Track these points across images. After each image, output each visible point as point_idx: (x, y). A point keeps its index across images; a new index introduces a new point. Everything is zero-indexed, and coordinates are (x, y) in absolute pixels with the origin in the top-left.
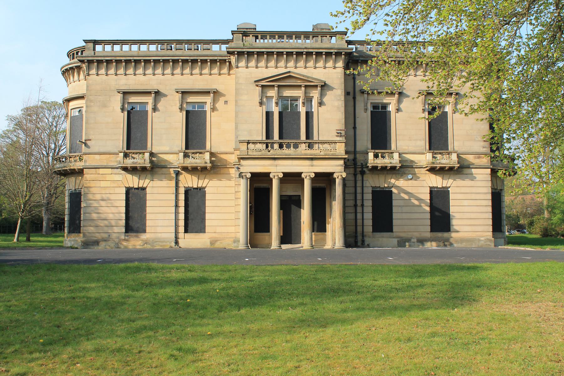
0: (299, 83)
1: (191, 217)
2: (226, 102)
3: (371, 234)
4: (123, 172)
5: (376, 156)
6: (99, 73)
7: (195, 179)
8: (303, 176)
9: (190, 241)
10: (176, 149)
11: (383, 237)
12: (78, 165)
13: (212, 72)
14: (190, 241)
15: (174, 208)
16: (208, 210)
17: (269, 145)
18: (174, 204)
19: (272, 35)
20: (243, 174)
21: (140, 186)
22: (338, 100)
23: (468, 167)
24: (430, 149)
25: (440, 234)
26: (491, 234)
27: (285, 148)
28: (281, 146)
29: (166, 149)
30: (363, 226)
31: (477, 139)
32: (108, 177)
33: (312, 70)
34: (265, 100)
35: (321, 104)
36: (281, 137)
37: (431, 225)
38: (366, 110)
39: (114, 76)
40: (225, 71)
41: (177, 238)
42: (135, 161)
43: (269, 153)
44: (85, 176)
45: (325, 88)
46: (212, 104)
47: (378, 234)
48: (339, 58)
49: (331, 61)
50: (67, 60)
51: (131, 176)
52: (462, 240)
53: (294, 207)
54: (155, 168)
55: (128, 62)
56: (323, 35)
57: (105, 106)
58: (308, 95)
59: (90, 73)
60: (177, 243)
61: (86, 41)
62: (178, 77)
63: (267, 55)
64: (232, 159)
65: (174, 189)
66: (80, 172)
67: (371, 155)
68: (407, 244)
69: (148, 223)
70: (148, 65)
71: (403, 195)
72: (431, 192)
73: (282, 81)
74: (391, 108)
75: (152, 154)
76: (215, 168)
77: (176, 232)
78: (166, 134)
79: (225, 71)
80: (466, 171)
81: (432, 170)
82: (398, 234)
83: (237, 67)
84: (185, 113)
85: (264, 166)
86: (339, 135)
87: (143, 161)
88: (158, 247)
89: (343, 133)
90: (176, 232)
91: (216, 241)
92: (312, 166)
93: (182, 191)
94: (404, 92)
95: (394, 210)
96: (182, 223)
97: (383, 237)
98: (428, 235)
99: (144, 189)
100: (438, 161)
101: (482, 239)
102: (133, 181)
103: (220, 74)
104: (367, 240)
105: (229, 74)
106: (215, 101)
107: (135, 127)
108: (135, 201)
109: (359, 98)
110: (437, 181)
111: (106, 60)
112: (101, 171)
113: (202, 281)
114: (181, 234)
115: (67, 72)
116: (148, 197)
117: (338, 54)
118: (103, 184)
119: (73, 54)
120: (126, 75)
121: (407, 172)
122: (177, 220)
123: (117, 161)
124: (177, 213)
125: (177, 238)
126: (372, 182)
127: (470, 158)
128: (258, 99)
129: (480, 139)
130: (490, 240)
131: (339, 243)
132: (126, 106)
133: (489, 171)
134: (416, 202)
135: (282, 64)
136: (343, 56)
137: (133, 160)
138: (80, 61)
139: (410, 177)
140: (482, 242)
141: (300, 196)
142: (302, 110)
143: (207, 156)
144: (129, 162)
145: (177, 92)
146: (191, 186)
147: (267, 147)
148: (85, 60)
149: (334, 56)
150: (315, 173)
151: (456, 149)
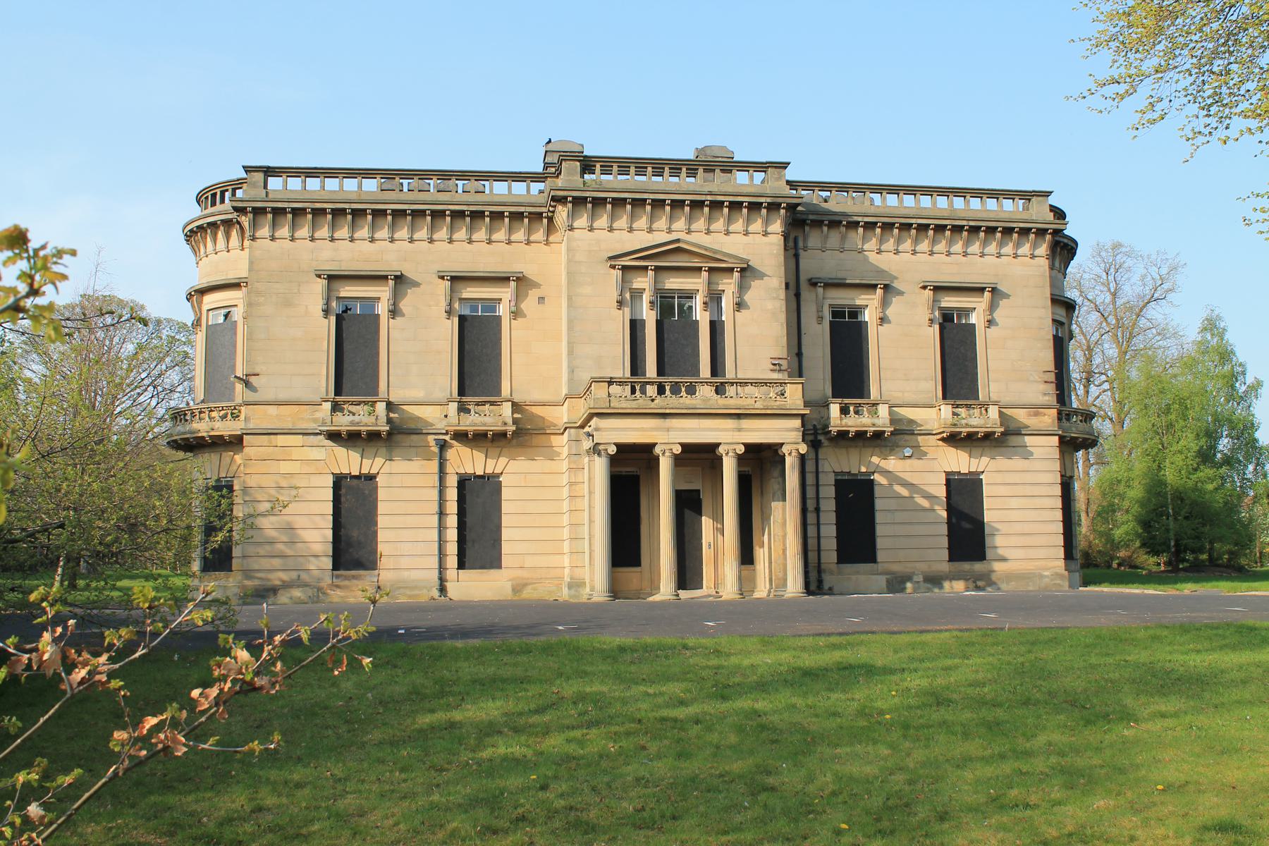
0: (696, 262)
1: (470, 536)
2: (541, 300)
3: (834, 567)
4: (329, 443)
5: (844, 411)
6: (277, 234)
7: (479, 456)
8: (657, 450)
9: (472, 587)
10: (441, 395)
11: (858, 573)
12: (226, 428)
13: (513, 238)
14: (472, 587)
15: (436, 517)
16: (505, 521)
17: (638, 388)
18: (435, 508)
19: (624, 165)
20: (601, 447)
21: (365, 471)
22: (775, 298)
23: (1018, 433)
24: (944, 398)
25: (966, 566)
26: (1061, 563)
27: (683, 393)
28: (661, 391)
29: (419, 394)
30: (819, 550)
32: (296, 453)
33: (721, 237)
35: (740, 306)
36: (661, 372)
37: (950, 548)
39: (347, 242)
40: (539, 235)
41: (442, 580)
42: (356, 418)
43: (653, 405)
44: (246, 450)
45: (748, 274)
46: (513, 303)
47: (848, 568)
48: (774, 215)
49: (760, 221)
50: (196, 211)
51: (343, 450)
52: (1010, 577)
54: (396, 435)
55: (338, 213)
56: (710, 167)
57: (288, 303)
58: (713, 287)
59: (258, 234)
60: (443, 590)
61: (248, 169)
62: (442, 246)
63: (633, 206)
64: (561, 415)
65: (437, 477)
66: (236, 442)
67: (835, 409)
68: (909, 585)
70: (439, 222)
71: (898, 488)
73: (664, 259)
74: (869, 316)
75: (390, 406)
76: (523, 435)
77: (440, 567)
78: (417, 363)
79: (539, 235)
80: (1014, 440)
81: (953, 439)
82: (886, 566)
83: (571, 229)
84: (456, 320)
85: (642, 429)
87: (372, 419)
88: (403, 600)
89: (784, 364)
90: (442, 568)
91: (525, 585)
92: (740, 430)
93: (452, 481)
94: (895, 284)
95: (879, 517)
96: (452, 548)
97: (858, 573)
98: (945, 567)
99: (371, 478)
102: (350, 461)
103: (528, 243)
104: (828, 581)
105: (547, 243)
106: (519, 297)
107: (354, 351)
108: (353, 505)
109: (806, 294)
110: (960, 461)
111: (293, 209)
112: (281, 440)
113: (849, 673)
115: (195, 234)
116: (381, 494)
117: (773, 207)
118: (285, 467)
119: (214, 195)
120: (332, 239)
121: (901, 443)
122: (442, 542)
123: (315, 420)
124: (442, 528)
125: (442, 580)
127: (1021, 415)
128: (615, 295)
130: (1061, 576)
131: (794, 585)
132: (334, 304)
133: (1055, 440)
134: (925, 503)
135: (662, 223)
136: (783, 212)
137: (351, 418)
138: (236, 209)
139: (908, 452)
141: (698, 491)
142: (702, 316)
143: (507, 409)
144: (343, 422)
145: (442, 278)
146: (346, 471)
147: (633, 391)
148: (241, 208)
149: (687, 209)
150: (745, 445)
151: (994, 397)
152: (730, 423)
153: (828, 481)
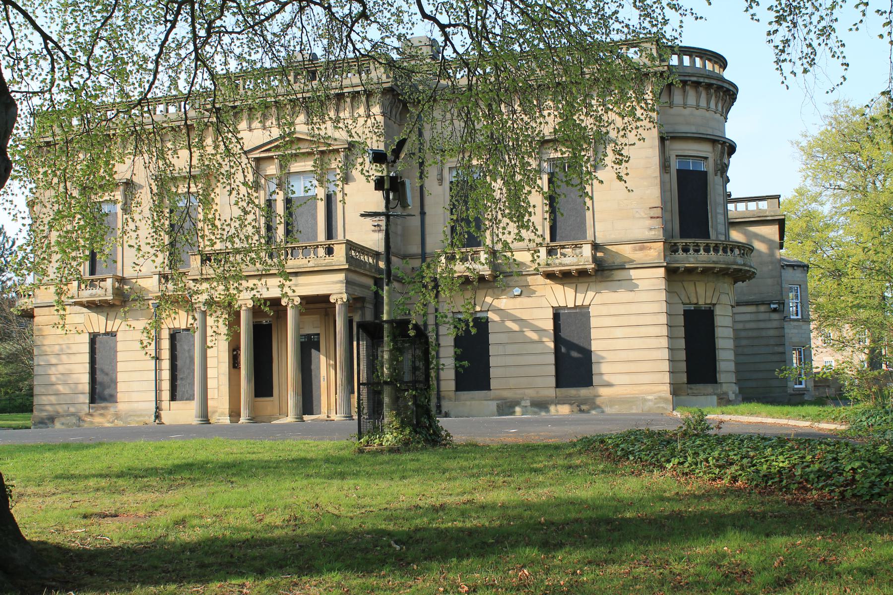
3: (452, 394)
11: (473, 399)
25: (572, 392)
31: (637, 215)
34: (263, 181)
37: (689, 372)
38: (441, 180)
41: (158, 408)
44: (36, 319)
53: (313, 351)
54: (123, 300)
60: (158, 416)
69: (120, 387)
72: (556, 317)
75: (596, 247)
86: (376, 228)
90: (158, 400)
93: (165, 334)
95: (492, 350)
96: (166, 385)
97: (473, 400)
99: (113, 334)
100: (557, 261)
101: (650, 397)
104: (446, 406)
114: (165, 404)
116: (120, 347)
125: (158, 408)
129: (643, 214)
130: (665, 400)
133: (661, 272)
139: (517, 291)
140: (650, 403)
146: (563, 304)
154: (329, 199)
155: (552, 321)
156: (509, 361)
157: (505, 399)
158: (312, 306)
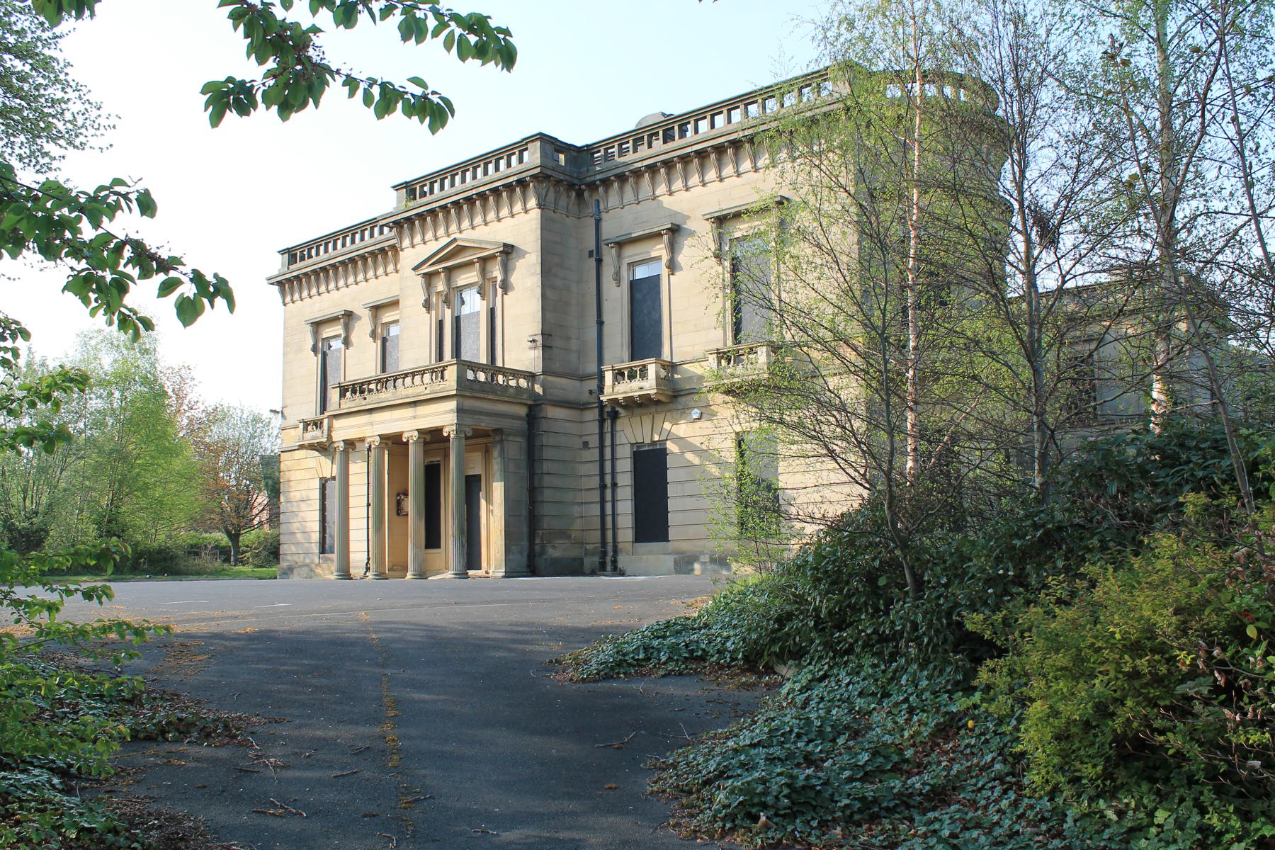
11: (651, 553)
39: (683, 192)
47: (644, 547)
68: (697, 566)
71: (690, 456)
92: (415, 417)
97: (652, 553)
104: (623, 561)
121: (692, 404)
126: (632, 432)
134: (714, 470)
139: (695, 413)
152: (409, 412)
153: (624, 453)
154: (492, 313)
155: (351, 494)
156: (690, 503)
157: (683, 553)
158: (473, 441)
